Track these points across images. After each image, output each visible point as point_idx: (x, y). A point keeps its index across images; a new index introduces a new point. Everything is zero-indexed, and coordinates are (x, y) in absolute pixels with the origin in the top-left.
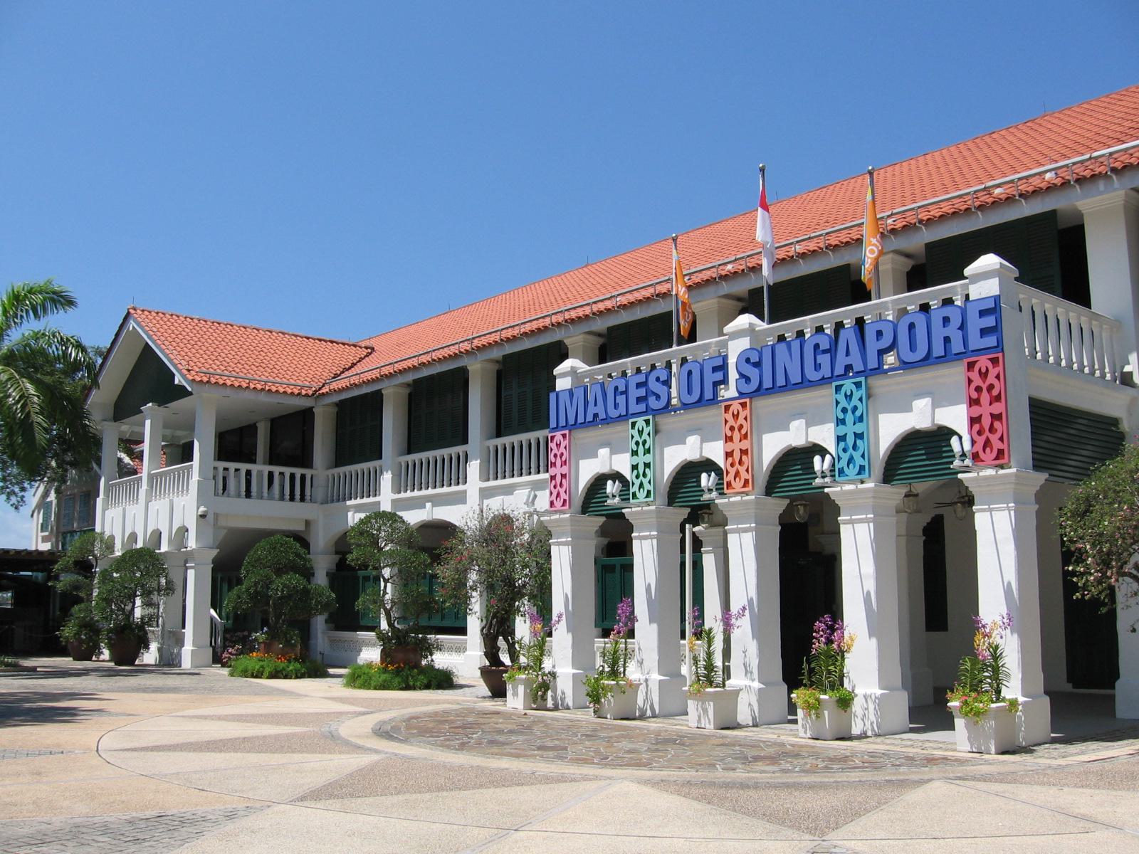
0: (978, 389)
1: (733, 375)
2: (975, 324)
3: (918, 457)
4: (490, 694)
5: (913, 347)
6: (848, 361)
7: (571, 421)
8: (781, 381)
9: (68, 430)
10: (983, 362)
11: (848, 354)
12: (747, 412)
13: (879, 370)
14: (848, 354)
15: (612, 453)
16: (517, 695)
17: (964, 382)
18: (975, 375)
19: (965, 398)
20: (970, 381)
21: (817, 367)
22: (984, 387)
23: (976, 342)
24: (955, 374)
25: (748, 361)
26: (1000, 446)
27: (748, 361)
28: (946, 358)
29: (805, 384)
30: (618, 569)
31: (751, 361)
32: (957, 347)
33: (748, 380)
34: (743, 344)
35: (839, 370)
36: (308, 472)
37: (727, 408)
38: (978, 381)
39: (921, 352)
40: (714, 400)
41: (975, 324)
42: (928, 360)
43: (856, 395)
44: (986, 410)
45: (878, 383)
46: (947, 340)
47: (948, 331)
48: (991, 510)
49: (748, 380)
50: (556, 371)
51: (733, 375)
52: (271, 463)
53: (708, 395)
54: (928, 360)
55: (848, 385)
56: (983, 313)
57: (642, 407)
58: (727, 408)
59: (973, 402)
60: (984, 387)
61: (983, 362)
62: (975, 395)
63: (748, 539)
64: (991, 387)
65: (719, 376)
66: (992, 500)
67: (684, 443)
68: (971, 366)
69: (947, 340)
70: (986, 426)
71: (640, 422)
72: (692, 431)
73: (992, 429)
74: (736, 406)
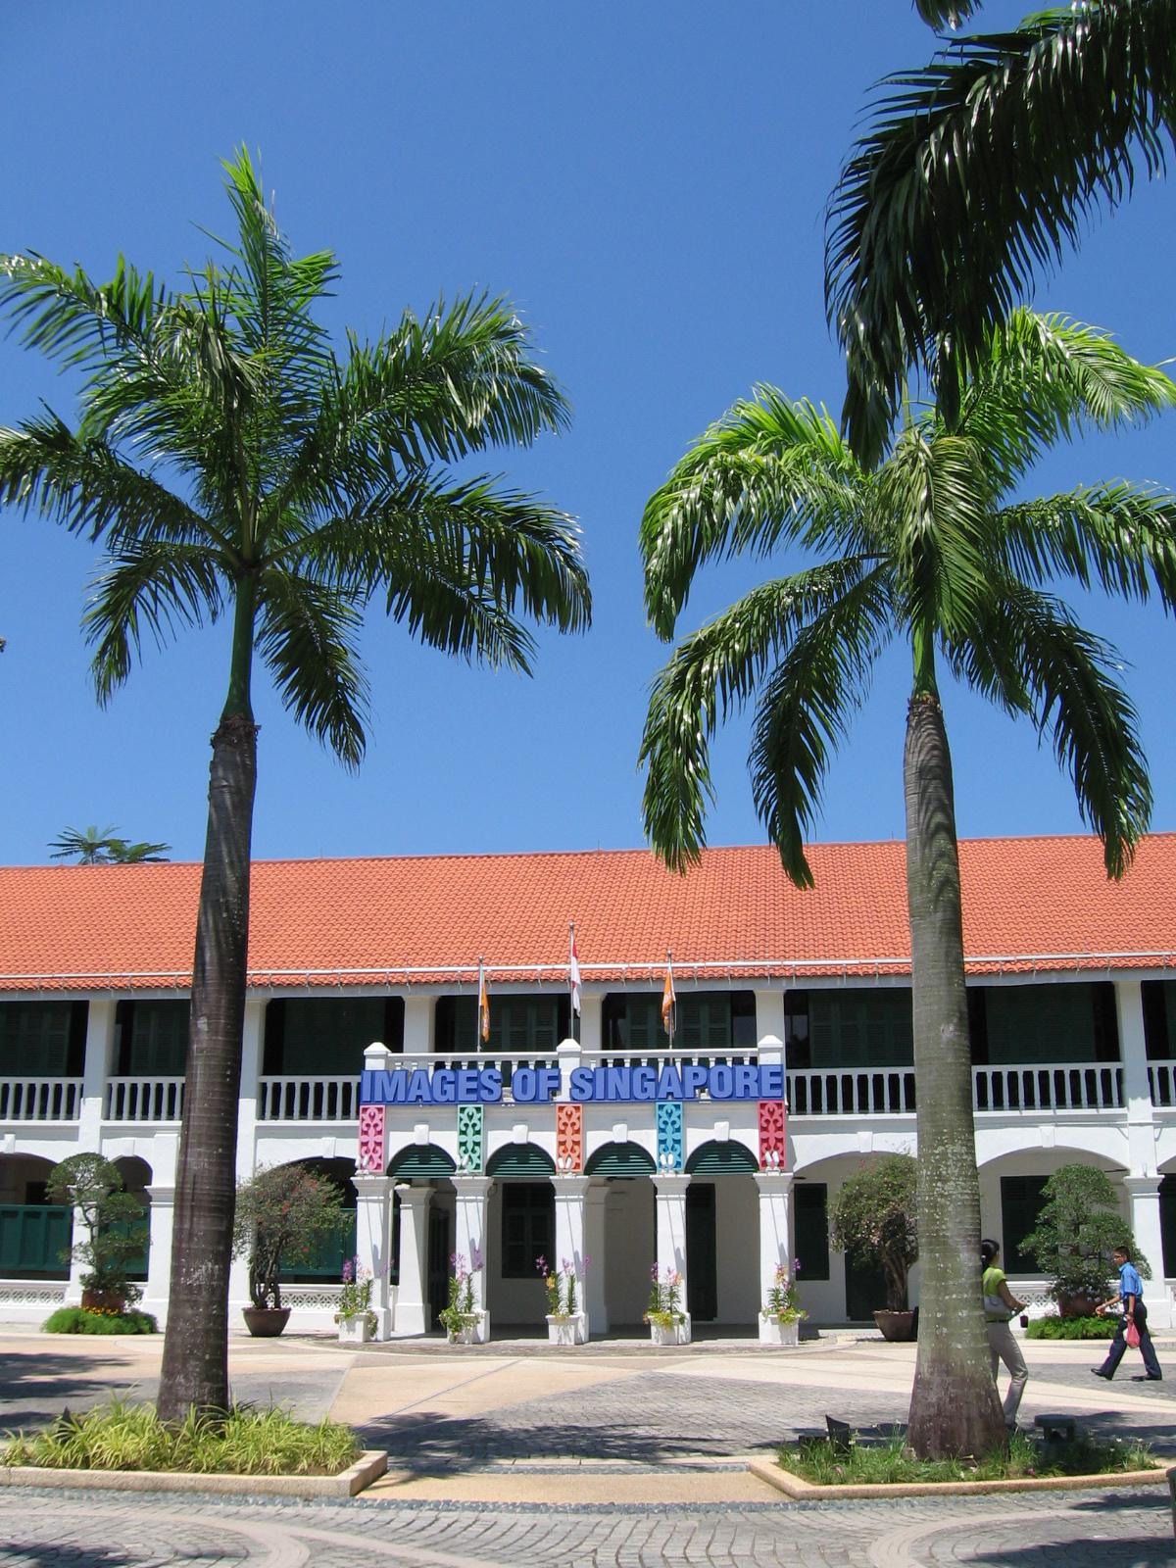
0: (767, 1121)
1: (566, 1085)
2: (767, 1080)
3: (413, 1163)
4: (249, 1333)
5: (721, 1087)
6: (419, 1093)
7: (390, 1098)
8: (612, 1095)
9: (235, 405)
10: (771, 1105)
11: (669, 1084)
12: (481, 1115)
13: (694, 1099)
14: (669, 1084)
15: (16, 1138)
16: (354, 1330)
17: (758, 1116)
18: (765, 1112)
19: (757, 1125)
20: (762, 1116)
21: (444, 1092)
22: (470, 1124)
23: (767, 1091)
24: (751, 1109)
25: (582, 1076)
26: (478, 1162)
27: (582, 1076)
28: (746, 1097)
29: (632, 1099)
30: (44, 1217)
31: (582, 1077)
32: (754, 1092)
33: (582, 1091)
34: (574, 1063)
35: (662, 1095)
36: (1113, 1066)
37: (561, 1109)
38: (767, 1116)
39: (727, 1092)
40: (548, 1102)
41: (767, 1080)
42: (732, 1097)
43: (477, 1116)
44: (772, 1135)
45: (691, 1108)
46: (747, 1087)
47: (748, 1082)
48: (771, 1197)
49: (582, 1091)
50: (367, 1052)
51: (566, 1085)
52: (605, 1047)
53: (543, 1095)
54: (731, 1097)
55: (669, 1106)
56: (772, 1074)
57: (473, 1097)
58: (561, 1109)
59: (763, 1129)
60: (470, 1124)
61: (771, 1105)
62: (765, 1125)
63: (576, 1209)
64: (474, 1125)
65: (554, 1084)
66: (771, 1191)
67: (511, 1129)
68: (763, 1106)
69: (747, 1087)
70: (371, 1148)
71: (470, 1109)
72: (623, 1120)
73: (473, 1151)
74: (569, 1108)
